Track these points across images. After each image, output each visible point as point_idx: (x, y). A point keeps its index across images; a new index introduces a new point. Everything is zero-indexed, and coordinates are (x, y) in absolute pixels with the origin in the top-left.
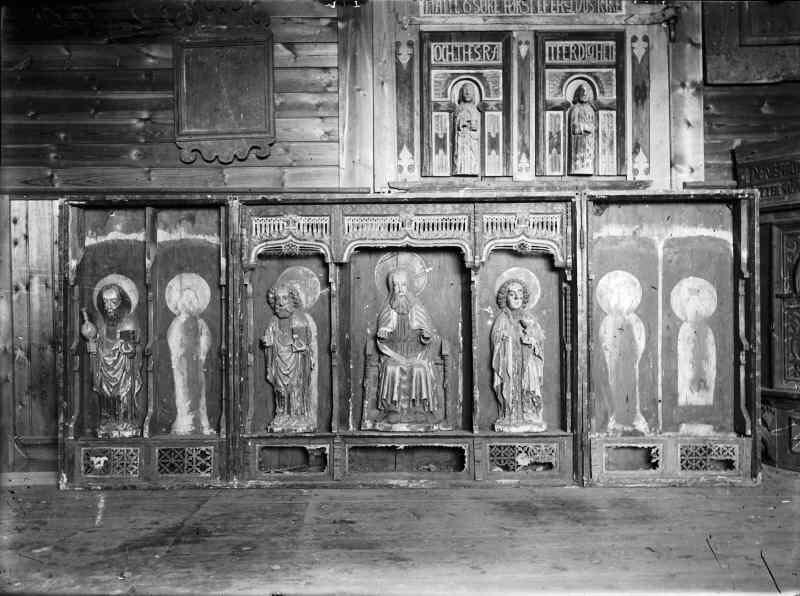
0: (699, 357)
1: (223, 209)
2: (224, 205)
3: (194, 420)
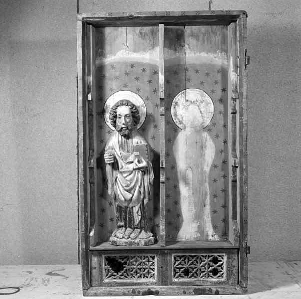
3: (199, 227)
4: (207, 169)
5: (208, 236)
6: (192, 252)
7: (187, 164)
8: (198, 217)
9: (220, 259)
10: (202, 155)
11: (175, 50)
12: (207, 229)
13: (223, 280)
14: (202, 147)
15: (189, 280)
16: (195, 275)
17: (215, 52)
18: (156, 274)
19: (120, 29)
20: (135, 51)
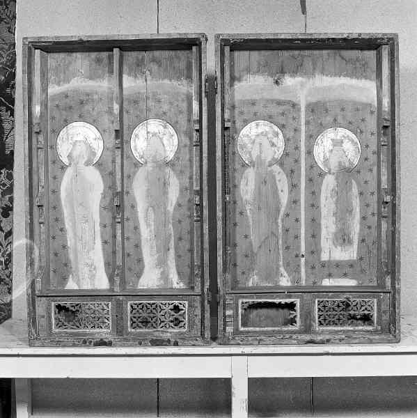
0: (343, 212)
1: (194, 48)
2: (196, 45)
3: (162, 273)
4: (171, 208)
5: (172, 284)
6: (151, 299)
7: (148, 202)
8: (162, 263)
9: (181, 307)
10: (165, 193)
11: (136, 77)
12: (171, 276)
13: (184, 330)
14: (165, 184)
15: (147, 330)
16: (154, 325)
17: (179, 78)
18: (110, 325)
19: (74, 54)
20: (91, 78)
